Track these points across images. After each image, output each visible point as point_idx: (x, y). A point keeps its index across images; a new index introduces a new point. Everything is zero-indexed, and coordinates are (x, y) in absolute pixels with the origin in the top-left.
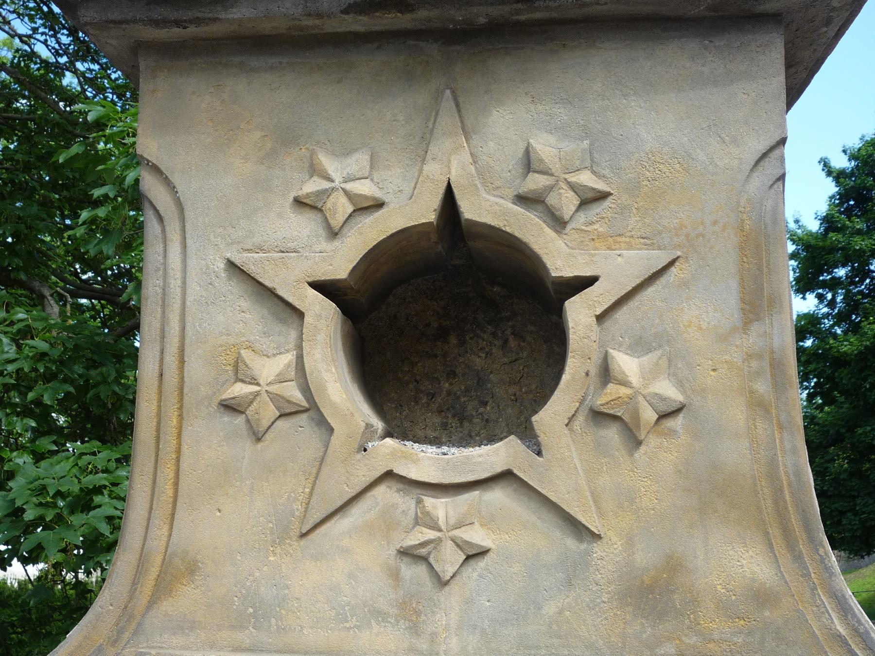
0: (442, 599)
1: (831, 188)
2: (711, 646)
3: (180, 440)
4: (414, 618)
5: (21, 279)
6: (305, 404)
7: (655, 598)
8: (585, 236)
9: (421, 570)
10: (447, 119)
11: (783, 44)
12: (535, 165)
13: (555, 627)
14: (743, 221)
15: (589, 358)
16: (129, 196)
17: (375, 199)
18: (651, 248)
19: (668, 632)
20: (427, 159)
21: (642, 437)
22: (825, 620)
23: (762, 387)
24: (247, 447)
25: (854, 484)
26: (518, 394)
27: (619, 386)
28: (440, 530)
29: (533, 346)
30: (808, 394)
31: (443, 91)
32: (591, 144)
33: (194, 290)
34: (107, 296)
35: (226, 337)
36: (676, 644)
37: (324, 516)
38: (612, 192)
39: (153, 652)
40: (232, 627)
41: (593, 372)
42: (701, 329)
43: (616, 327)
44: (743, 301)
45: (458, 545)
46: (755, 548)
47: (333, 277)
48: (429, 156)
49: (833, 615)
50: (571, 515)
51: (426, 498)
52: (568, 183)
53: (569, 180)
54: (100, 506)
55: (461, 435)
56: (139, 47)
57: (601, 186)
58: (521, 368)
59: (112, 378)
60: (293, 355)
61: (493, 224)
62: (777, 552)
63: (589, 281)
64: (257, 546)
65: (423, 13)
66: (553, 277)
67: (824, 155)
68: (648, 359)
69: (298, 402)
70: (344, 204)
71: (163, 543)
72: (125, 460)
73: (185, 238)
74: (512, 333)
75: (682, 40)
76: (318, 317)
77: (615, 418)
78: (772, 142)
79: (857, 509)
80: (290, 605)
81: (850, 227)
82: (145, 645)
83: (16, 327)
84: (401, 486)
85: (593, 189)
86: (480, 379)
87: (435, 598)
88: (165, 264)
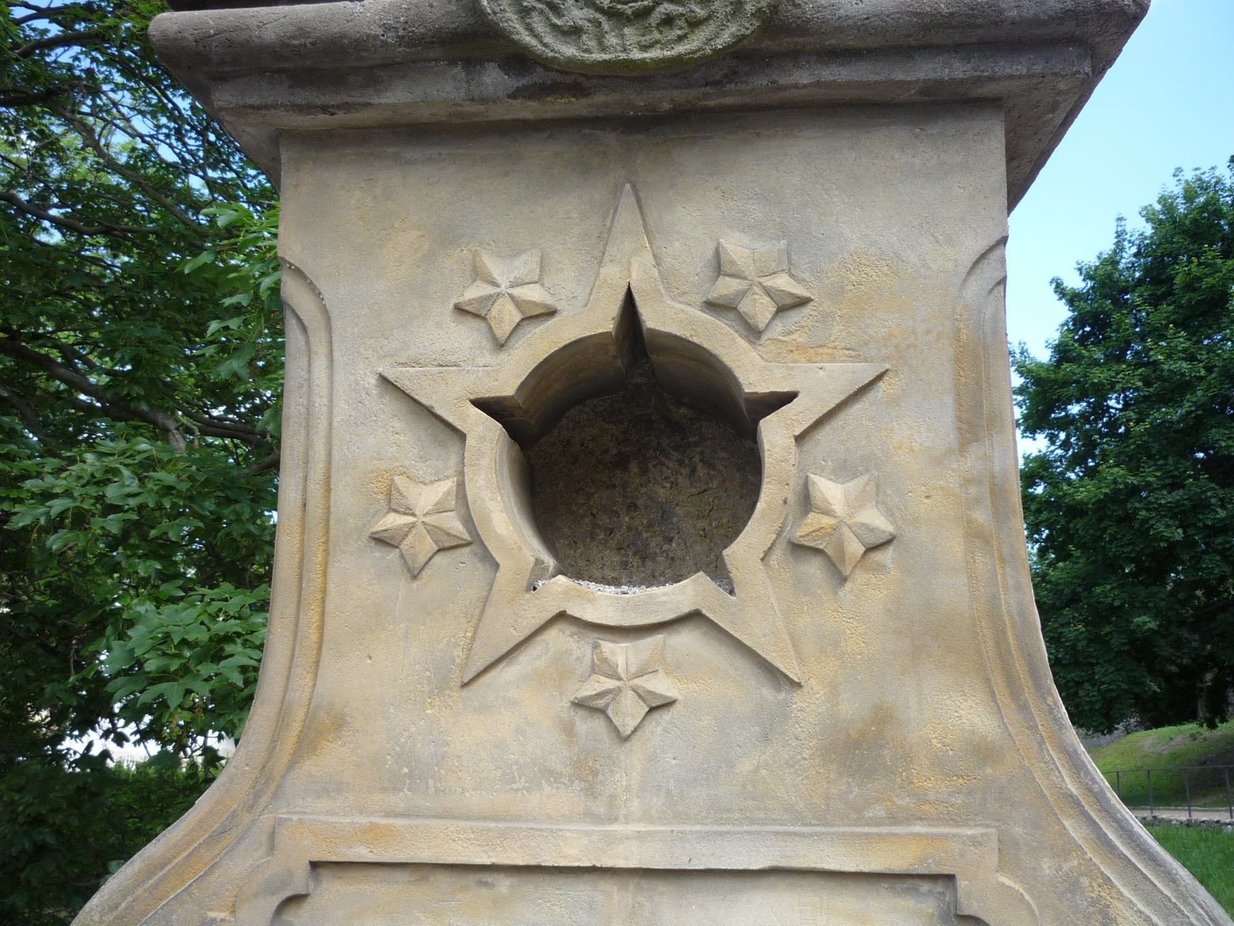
0: (622, 758)
1: (1064, 313)
2: (926, 807)
3: (326, 578)
4: (590, 778)
5: (143, 410)
6: (467, 537)
7: (863, 754)
8: (782, 347)
9: (598, 724)
10: (627, 216)
11: (1003, 132)
12: (726, 267)
13: (750, 788)
14: (959, 330)
15: (787, 484)
16: (266, 307)
17: (545, 306)
18: (857, 360)
19: (877, 792)
20: (604, 261)
21: (848, 573)
22: (1054, 778)
23: (982, 516)
24: (401, 587)
25: (1092, 650)
26: (707, 529)
27: (821, 515)
28: (620, 679)
29: (725, 475)
30: (1040, 549)
31: (622, 186)
32: (789, 244)
33: (342, 408)
34: (240, 434)
35: (377, 462)
36: (886, 806)
37: (488, 663)
38: (812, 297)
39: (295, 818)
40: (384, 789)
41: (792, 499)
42: (913, 451)
43: (817, 450)
44: (960, 419)
45: (640, 696)
46: (975, 696)
47: (498, 394)
48: (607, 258)
49: (1064, 772)
50: (767, 661)
51: (604, 642)
52: (763, 287)
53: (764, 284)
54: (232, 655)
55: (643, 575)
56: (281, 136)
57: (800, 291)
58: (711, 500)
59: (246, 516)
60: (453, 482)
61: (678, 334)
62: (999, 702)
63: (787, 398)
64: (412, 697)
65: (599, 98)
66: (746, 393)
67: (1056, 274)
68: (855, 485)
69: (458, 535)
70: (510, 311)
71: (306, 694)
72: (263, 606)
73: (331, 351)
74: (701, 461)
75: (891, 128)
76: (482, 439)
77: (817, 551)
78: (992, 241)
79: (1096, 678)
80: (450, 764)
81: (1087, 357)
82: (285, 810)
83: (138, 458)
84: (574, 629)
85: (792, 294)
86: (664, 512)
87: (614, 755)
88: (309, 380)
